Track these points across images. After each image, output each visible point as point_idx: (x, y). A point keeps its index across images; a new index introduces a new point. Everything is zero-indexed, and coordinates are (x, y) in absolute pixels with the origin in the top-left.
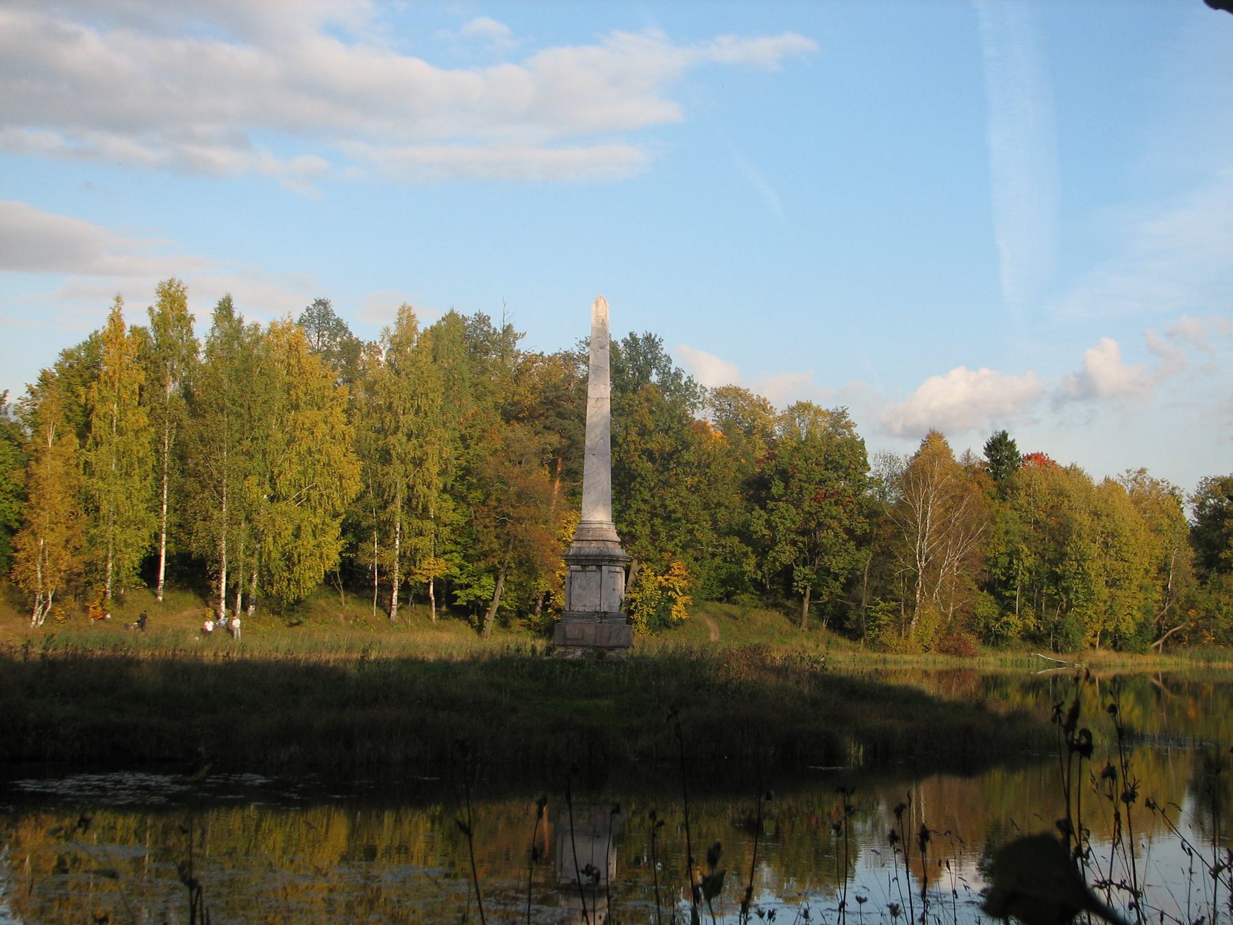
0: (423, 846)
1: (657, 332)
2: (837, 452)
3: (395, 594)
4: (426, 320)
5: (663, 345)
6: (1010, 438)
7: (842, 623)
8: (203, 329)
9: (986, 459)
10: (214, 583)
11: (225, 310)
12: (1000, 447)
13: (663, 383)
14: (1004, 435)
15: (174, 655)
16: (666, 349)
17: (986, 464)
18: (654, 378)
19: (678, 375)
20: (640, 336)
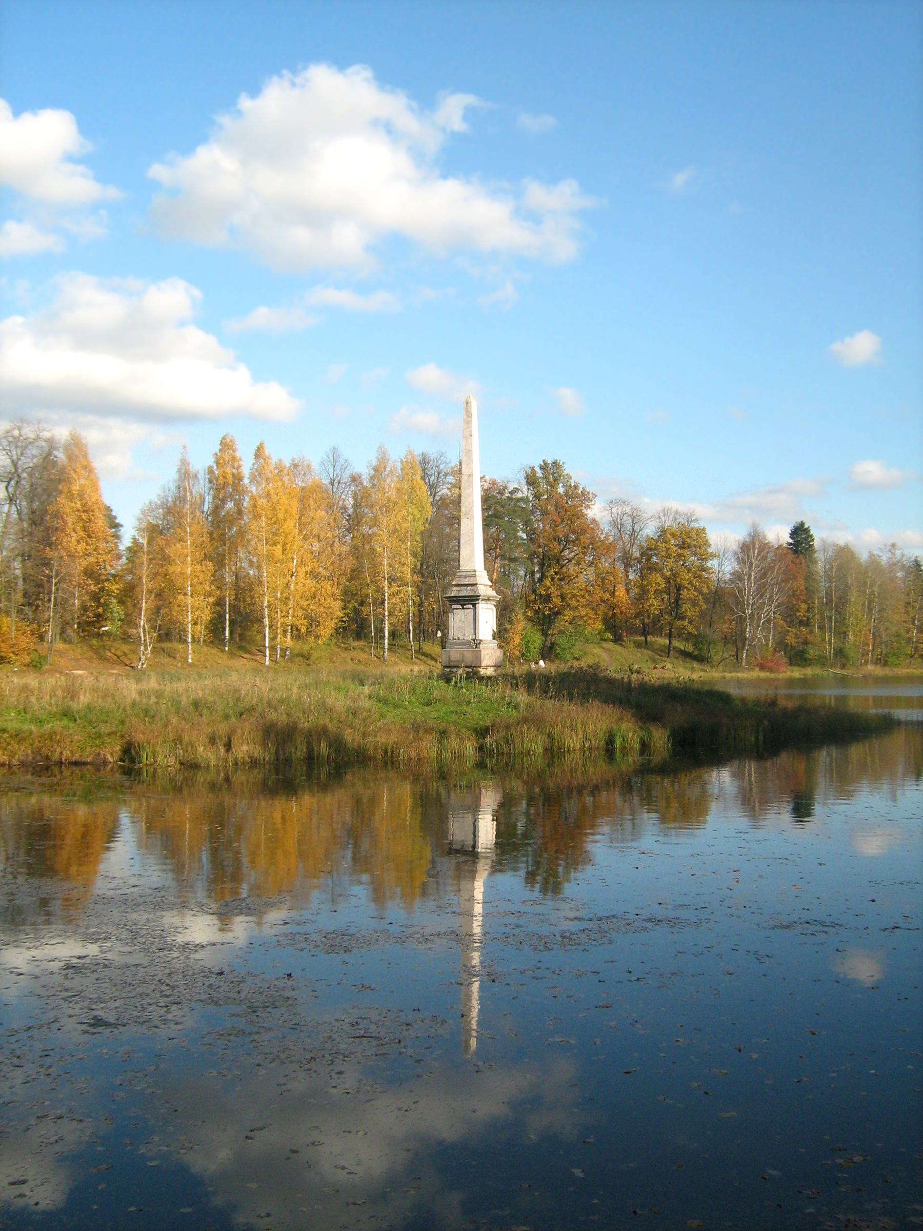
0: (405, 798)
1: (561, 459)
2: (687, 540)
3: (386, 641)
4: (396, 456)
5: (565, 466)
6: (806, 526)
7: (771, 671)
8: (247, 466)
9: (791, 541)
10: (259, 637)
11: (259, 453)
12: (800, 533)
13: (566, 494)
14: (802, 524)
15: (643, 779)
16: (567, 469)
17: (791, 544)
18: (561, 490)
19: (576, 487)
20: (550, 462)
